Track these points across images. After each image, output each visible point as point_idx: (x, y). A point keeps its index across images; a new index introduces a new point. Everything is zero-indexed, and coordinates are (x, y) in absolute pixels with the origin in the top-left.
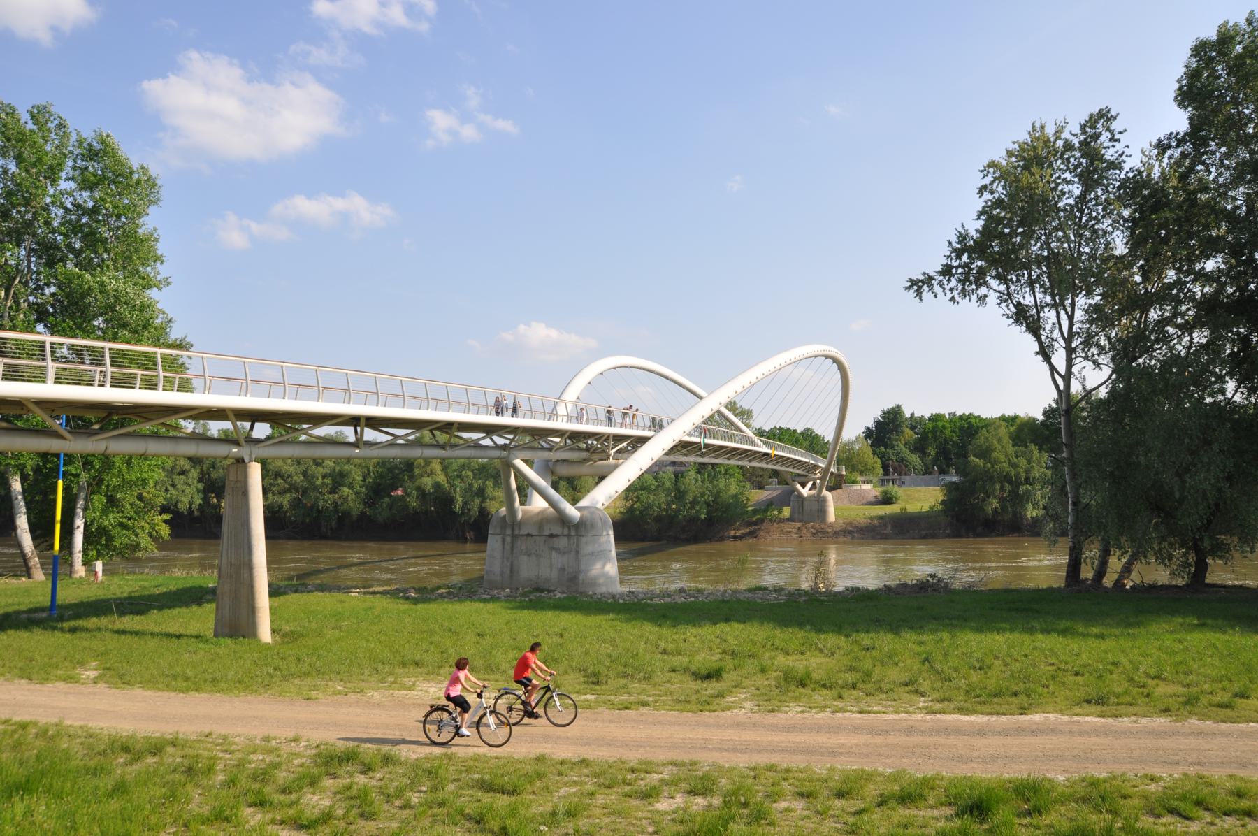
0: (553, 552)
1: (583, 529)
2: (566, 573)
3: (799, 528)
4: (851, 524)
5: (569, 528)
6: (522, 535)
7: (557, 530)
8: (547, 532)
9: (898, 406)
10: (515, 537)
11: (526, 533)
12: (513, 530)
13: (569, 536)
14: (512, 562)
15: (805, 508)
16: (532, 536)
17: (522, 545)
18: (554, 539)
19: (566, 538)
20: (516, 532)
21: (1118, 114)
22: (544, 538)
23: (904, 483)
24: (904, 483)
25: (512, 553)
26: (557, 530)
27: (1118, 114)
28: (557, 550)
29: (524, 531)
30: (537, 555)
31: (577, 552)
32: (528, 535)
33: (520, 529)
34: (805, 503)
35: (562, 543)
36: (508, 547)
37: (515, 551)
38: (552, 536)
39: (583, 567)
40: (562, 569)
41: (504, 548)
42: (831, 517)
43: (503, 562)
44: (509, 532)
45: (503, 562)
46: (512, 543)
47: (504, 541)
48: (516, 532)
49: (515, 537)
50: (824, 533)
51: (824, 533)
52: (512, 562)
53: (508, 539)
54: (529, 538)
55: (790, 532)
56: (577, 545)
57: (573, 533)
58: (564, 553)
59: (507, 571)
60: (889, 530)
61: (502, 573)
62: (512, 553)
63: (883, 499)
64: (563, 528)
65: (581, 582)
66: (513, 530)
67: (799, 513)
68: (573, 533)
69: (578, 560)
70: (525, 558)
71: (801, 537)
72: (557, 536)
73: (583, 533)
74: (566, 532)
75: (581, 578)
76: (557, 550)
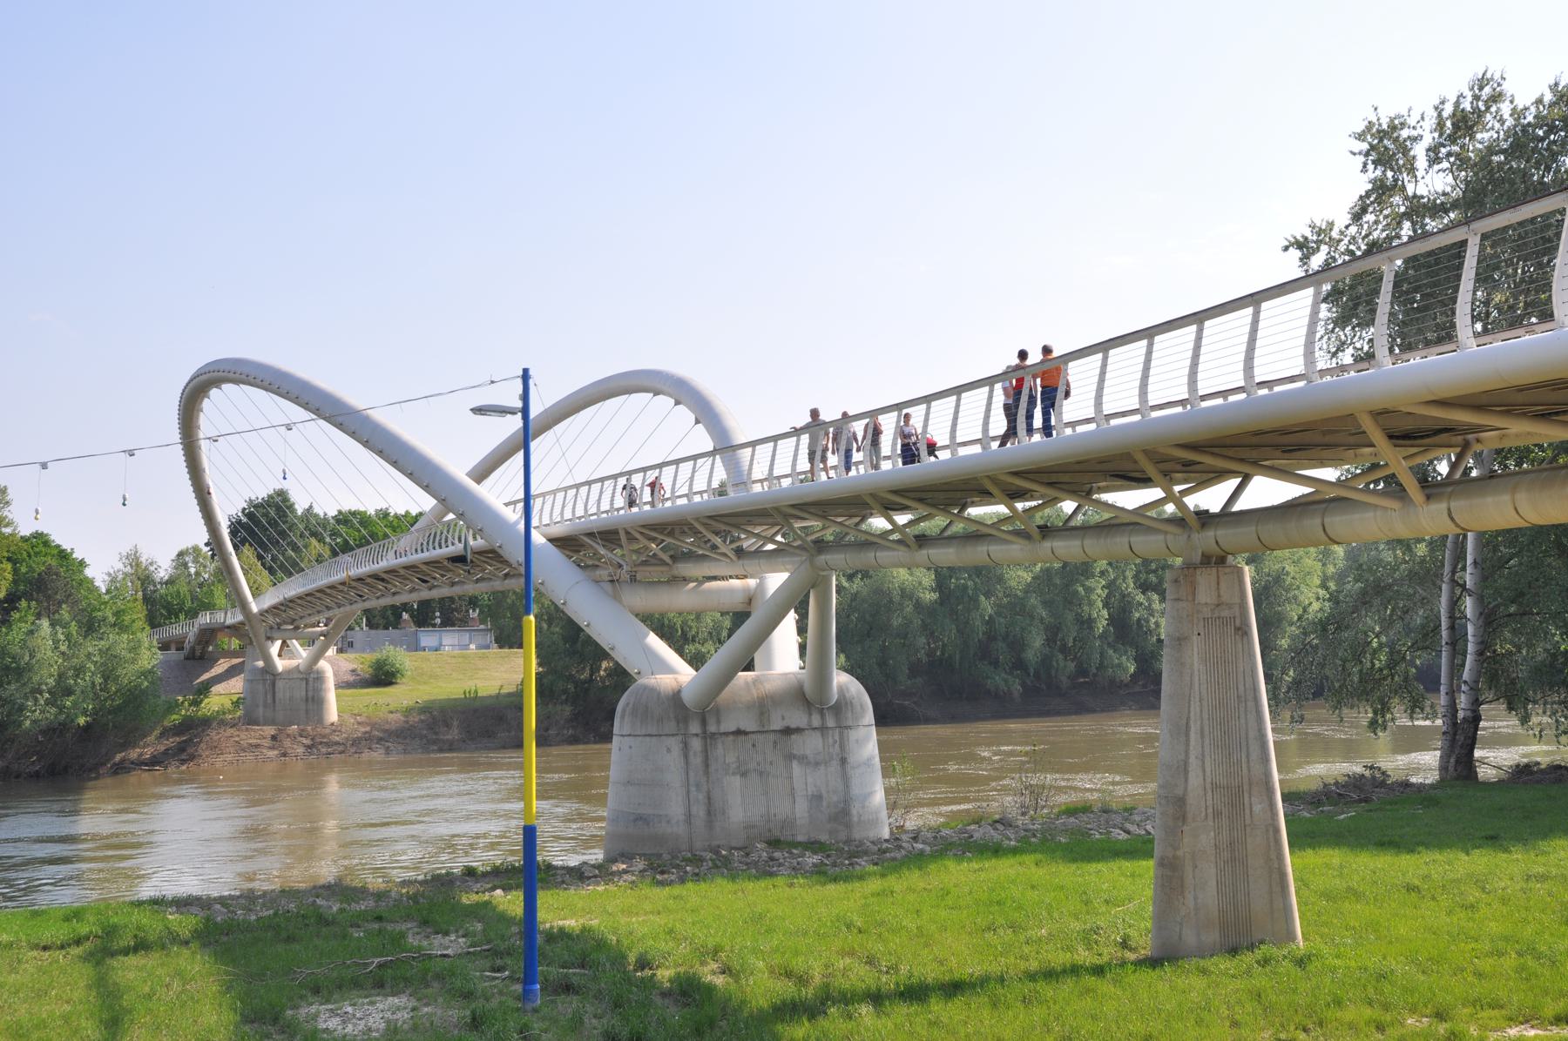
0: (795, 764)
1: (850, 714)
2: (825, 804)
3: (274, 738)
4: (373, 725)
5: (821, 712)
6: (726, 734)
7: (797, 718)
8: (777, 724)
9: (282, 494)
10: (709, 738)
11: (733, 729)
12: (704, 723)
13: (823, 729)
14: (709, 792)
15: (279, 695)
16: (745, 733)
17: (726, 754)
18: (793, 737)
19: (818, 734)
20: (712, 728)
21: (1286, 249)
22: (772, 737)
23: (351, 645)
24: (351, 645)
25: (707, 772)
26: (797, 718)
27: (1286, 249)
28: (803, 759)
29: (729, 725)
30: (761, 774)
31: (843, 761)
32: (739, 732)
33: (718, 722)
34: (280, 684)
35: (811, 744)
36: (697, 761)
37: (712, 769)
38: (788, 731)
39: (856, 790)
40: (817, 798)
41: (687, 763)
42: (332, 714)
43: (688, 792)
44: (695, 728)
45: (688, 792)
46: (705, 751)
47: (686, 746)
48: (712, 728)
49: (709, 738)
50: (327, 745)
51: (327, 745)
52: (709, 792)
53: (696, 744)
54: (742, 738)
55: (257, 746)
56: (842, 747)
57: (831, 723)
58: (817, 764)
59: (699, 811)
60: (454, 734)
61: (689, 817)
62: (707, 772)
63: (376, 676)
64: (810, 715)
65: (855, 819)
66: (704, 723)
67: (265, 706)
68: (831, 723)
69: (846, 779)
70: (736, 781)
71: (284, 755)
72: (798, 730)
73: (850, 723)
74: (816, 722)
75: (854, 812)
76: (803, 759)
